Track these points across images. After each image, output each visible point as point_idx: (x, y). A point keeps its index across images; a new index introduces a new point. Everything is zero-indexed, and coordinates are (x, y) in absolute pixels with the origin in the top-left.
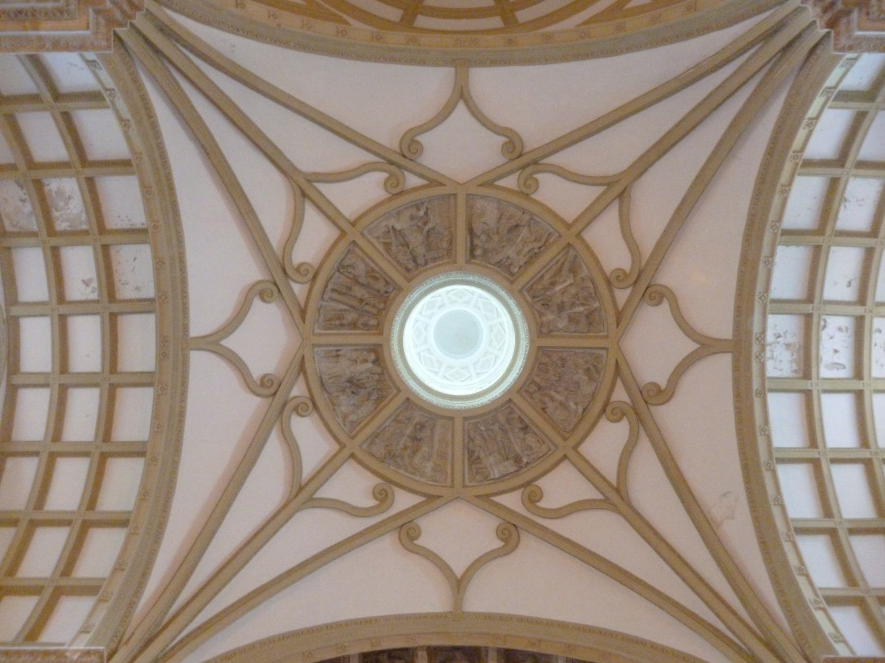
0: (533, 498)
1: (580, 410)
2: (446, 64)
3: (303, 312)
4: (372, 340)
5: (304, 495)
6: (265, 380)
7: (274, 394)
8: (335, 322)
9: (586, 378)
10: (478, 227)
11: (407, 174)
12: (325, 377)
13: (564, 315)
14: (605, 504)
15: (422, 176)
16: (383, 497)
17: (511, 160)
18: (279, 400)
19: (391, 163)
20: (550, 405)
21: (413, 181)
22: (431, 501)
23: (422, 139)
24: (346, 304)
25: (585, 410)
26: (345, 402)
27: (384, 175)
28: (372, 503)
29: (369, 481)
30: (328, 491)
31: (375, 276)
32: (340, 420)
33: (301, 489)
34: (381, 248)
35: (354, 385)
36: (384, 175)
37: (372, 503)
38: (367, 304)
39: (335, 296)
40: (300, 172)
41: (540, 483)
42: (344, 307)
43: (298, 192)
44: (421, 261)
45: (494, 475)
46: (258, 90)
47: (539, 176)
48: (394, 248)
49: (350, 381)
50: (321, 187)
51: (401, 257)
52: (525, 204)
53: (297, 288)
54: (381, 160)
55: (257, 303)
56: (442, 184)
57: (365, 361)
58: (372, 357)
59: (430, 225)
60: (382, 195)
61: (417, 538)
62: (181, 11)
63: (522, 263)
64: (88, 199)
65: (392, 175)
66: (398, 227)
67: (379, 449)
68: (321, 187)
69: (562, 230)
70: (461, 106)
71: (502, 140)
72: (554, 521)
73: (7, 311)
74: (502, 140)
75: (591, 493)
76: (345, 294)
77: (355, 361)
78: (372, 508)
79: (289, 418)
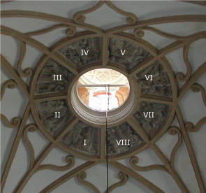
0: (134, 161)
1: (157, 127)
3: (28, 89)
5: (37, 166)
9: (161, 115)
12: (41, 114)
13: (154, 87)
14: (163, 168)
16: (70, 161)
18: (22, 128)
22: (89, 164)
25: (159, 127)
29: (63, 155)
30: (45, 162)
32: (49, 131)
33: (35, 163)
37: (65, 164)
48: (72, 57)
53: (25, 79)
56: (178, 95)
57: (60, 105)
58: (63, 103)
63: (134, 64)
64: (28, 178)
66: (73, 48)
67: (67, 141)
69: (154, 54)
75: (160, 162)
77: (54, 105)
78: (65, 166)
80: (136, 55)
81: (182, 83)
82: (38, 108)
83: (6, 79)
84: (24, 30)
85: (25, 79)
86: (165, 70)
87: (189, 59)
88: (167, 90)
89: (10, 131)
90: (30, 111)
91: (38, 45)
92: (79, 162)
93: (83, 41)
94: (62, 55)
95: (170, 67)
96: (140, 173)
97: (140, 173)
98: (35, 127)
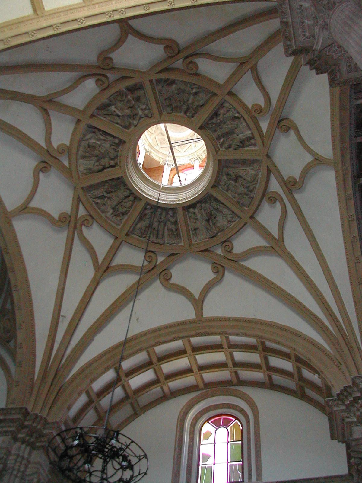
2: (12, 225)
4: (180, 213)
6: (215, 271)
7: (223, 267)
8: (176, 234)
10: (97, 166)
11: (79, 216)
14: (254, 69)
15: (78, 209)
16: (273, 199)
17: (50, 166)
18: (224, 263)
19: (75, 227)
20: (197, 103)
21: (82, 211)
23: (56, 216)
24: (164, 228)
26: (221, 222)
27: (84, 229)
28: (278, 204)
29: (266, 207)
31: (142, 217)
32: (233, 224)
34: (126, 217)
35: (210, 218)
36: (84, 229)
37: (278, 204)
38: (161, 218)
39: (160, 237)
40: (95, 275)
41: (250, 106)
42: (166, 230)
43: (106, 274)
44: (127, 193)
45: (249, 134)
46: (64, 289)
47: (55, 146)
49: (208, 221)
50: (100, 260)
51: (128, 204)
52: (74, 151)
53: (160, 259)
54: (76, 234)
55: (172, 281)
57: (194, 213)
59: (105, 194)
60: (95, 226)
61: (295, 179)
62: (34, 372)
65: (82, 224)
68: (100, 260)
70: (33, 204)
71: (41, 175)
72: (272, 100)
73: (202, 389)
74: (41, 175)
76: (158, 231)
79: (236, 254)
80: (99, 140)
81: (112, 76)
82: (201, 239)
83: (157, 284)
84: (90, 273)
85: (160, 259)
86: (104, 99)
87: (69, 84)
88: (132, 89)
89: (229, 276)
90: (206, 250)
91: (114, 251)
92: (275, 186)
93: (97, 203)
94: (124, 220)
95: (94, 98)
96: (274, 101)
97: (274, 101)
98: (227, 243)
